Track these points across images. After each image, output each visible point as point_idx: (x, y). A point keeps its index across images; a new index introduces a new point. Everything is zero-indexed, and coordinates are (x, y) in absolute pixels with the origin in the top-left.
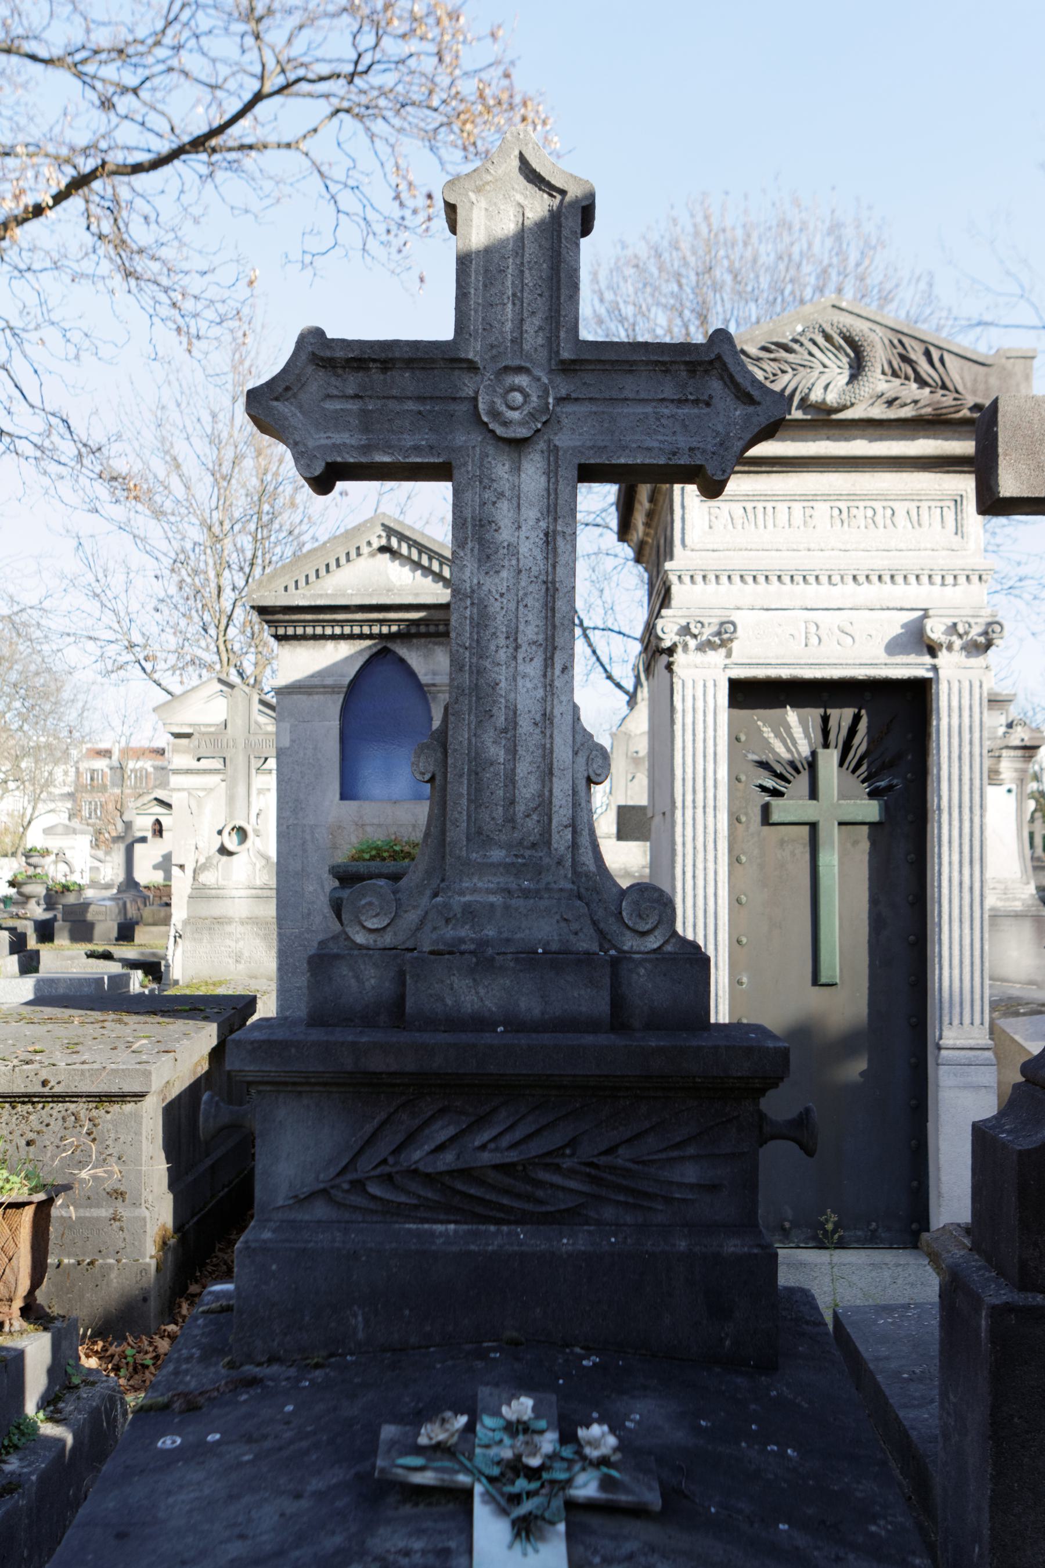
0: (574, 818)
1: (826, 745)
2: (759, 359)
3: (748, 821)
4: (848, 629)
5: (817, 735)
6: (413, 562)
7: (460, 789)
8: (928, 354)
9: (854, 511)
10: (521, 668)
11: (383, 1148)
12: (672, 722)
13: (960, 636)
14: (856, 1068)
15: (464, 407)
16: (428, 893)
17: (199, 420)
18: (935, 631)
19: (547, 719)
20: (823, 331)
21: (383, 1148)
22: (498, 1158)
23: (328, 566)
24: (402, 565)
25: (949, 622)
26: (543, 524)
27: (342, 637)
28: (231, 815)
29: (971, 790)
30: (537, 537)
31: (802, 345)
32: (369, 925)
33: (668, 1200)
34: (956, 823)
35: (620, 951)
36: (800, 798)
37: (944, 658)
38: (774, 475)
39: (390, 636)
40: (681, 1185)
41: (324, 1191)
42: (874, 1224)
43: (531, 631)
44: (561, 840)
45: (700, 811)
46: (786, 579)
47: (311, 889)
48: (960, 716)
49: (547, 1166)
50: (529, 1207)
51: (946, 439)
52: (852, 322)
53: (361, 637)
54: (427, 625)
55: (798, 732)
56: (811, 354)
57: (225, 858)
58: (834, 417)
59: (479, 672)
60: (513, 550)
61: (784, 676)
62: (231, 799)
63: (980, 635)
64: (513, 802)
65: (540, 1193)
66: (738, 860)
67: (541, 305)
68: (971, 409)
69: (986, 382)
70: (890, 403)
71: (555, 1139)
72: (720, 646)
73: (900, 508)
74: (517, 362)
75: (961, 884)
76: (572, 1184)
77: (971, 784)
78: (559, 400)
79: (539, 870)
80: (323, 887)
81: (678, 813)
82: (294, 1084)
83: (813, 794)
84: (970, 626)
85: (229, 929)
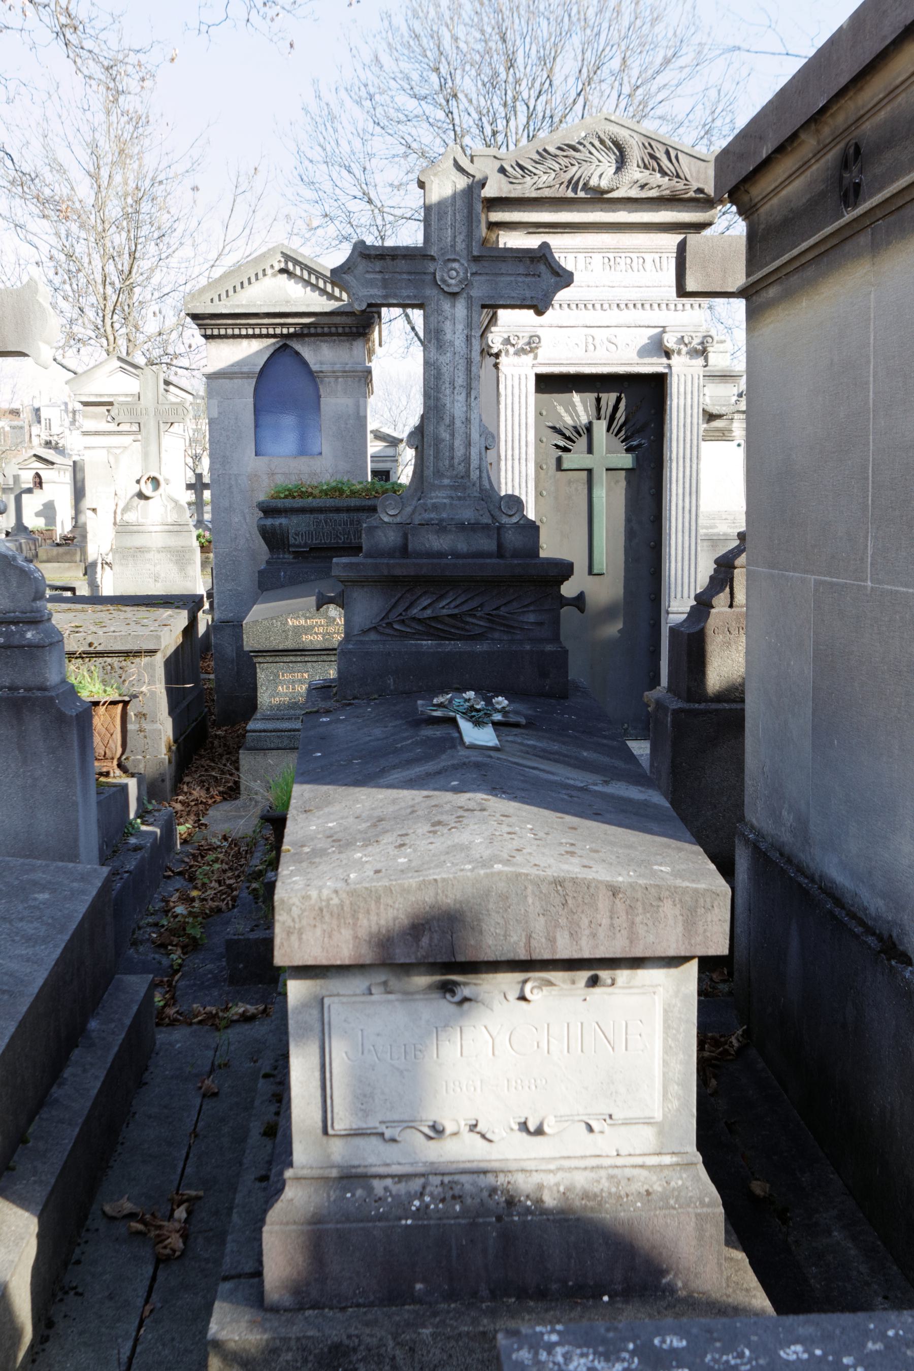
0: (480, 465)
1: (599, 418)
2: (556, 156)
3: (548, 468)
4: (614, 340)
5: (592, 411)
6: (305, 280)
7: (430, 452)
8: (668, 153)
9: (618, 260)
10: (456, 397)
11: (400, 609)
12: (498, 402)
13: (686, 345)
14: (613, 629)
15: (429, 277)
16: (416, 499)
17: (78, 130)
18: (670, 341)
19: (468, 421)
20: (599, 137)
21: (400, 609)
22: (450, 612)
23: (242, 283)
24: (296, 283)
25: (679, 335)
26: (465, 332)
27: (254, 336)
28: (146, 468)
29: (691, 447)
30: (463, 338)
31: (585, 146)
32: (390, 513)
33: (522, 629)
34: (681, 469)
35: (500, 523)
36: (582, 453)
37: (675, 360)
38: (565, 235)
39: (289, 336)
40: (527, 623)
41: (375, 627)
42: (626, 725)
43: (460, 380)
44: (474, 475)
45: (516, 462)
46: (574, 306)
47: (237, 520)
48: (685, 398)
49: (470, 615)
50: (463, 633)
51: (679, 211)
52: (618, 131)
53: (268, 336)
54: (316, 328)
55: (580, 408)
56: (590, 153)
57: (143, 502)
58: (606, 196)
59: (437, 399)
60: (452, 343)
61: (572, 372)
62: (146, 455)
63: (699, 344)
64: (453, 458)
65: (467, 627)
66: (541, 494)
67: (464, 229)
68: (695, 192)
69: (706, 173)
70: (642, 187)
71: (474, 603)
72: (530, 352)
73: (649, 257)
74: (453, 257)
75: (683, 508)
76: (482, 623)
77: (691, 443)
78: (472, 274)
79: (465, 489)
80: (245, 519)
81: (503, 463)
82: (361, 582)
83: (590, 450)
84: (692, 338)
85: (148, 556)
